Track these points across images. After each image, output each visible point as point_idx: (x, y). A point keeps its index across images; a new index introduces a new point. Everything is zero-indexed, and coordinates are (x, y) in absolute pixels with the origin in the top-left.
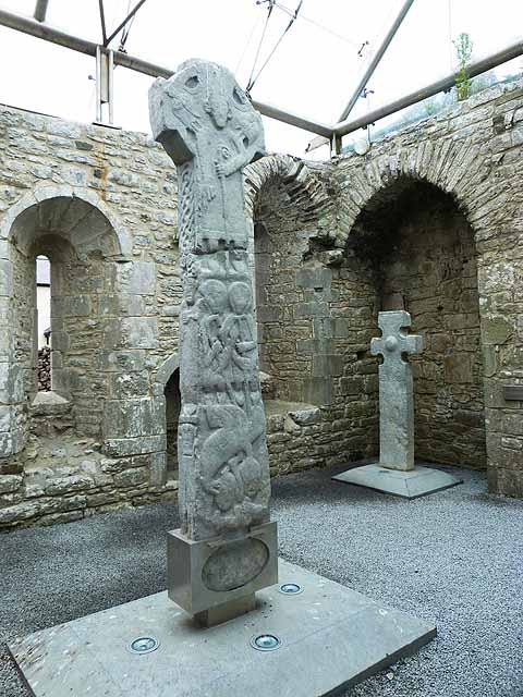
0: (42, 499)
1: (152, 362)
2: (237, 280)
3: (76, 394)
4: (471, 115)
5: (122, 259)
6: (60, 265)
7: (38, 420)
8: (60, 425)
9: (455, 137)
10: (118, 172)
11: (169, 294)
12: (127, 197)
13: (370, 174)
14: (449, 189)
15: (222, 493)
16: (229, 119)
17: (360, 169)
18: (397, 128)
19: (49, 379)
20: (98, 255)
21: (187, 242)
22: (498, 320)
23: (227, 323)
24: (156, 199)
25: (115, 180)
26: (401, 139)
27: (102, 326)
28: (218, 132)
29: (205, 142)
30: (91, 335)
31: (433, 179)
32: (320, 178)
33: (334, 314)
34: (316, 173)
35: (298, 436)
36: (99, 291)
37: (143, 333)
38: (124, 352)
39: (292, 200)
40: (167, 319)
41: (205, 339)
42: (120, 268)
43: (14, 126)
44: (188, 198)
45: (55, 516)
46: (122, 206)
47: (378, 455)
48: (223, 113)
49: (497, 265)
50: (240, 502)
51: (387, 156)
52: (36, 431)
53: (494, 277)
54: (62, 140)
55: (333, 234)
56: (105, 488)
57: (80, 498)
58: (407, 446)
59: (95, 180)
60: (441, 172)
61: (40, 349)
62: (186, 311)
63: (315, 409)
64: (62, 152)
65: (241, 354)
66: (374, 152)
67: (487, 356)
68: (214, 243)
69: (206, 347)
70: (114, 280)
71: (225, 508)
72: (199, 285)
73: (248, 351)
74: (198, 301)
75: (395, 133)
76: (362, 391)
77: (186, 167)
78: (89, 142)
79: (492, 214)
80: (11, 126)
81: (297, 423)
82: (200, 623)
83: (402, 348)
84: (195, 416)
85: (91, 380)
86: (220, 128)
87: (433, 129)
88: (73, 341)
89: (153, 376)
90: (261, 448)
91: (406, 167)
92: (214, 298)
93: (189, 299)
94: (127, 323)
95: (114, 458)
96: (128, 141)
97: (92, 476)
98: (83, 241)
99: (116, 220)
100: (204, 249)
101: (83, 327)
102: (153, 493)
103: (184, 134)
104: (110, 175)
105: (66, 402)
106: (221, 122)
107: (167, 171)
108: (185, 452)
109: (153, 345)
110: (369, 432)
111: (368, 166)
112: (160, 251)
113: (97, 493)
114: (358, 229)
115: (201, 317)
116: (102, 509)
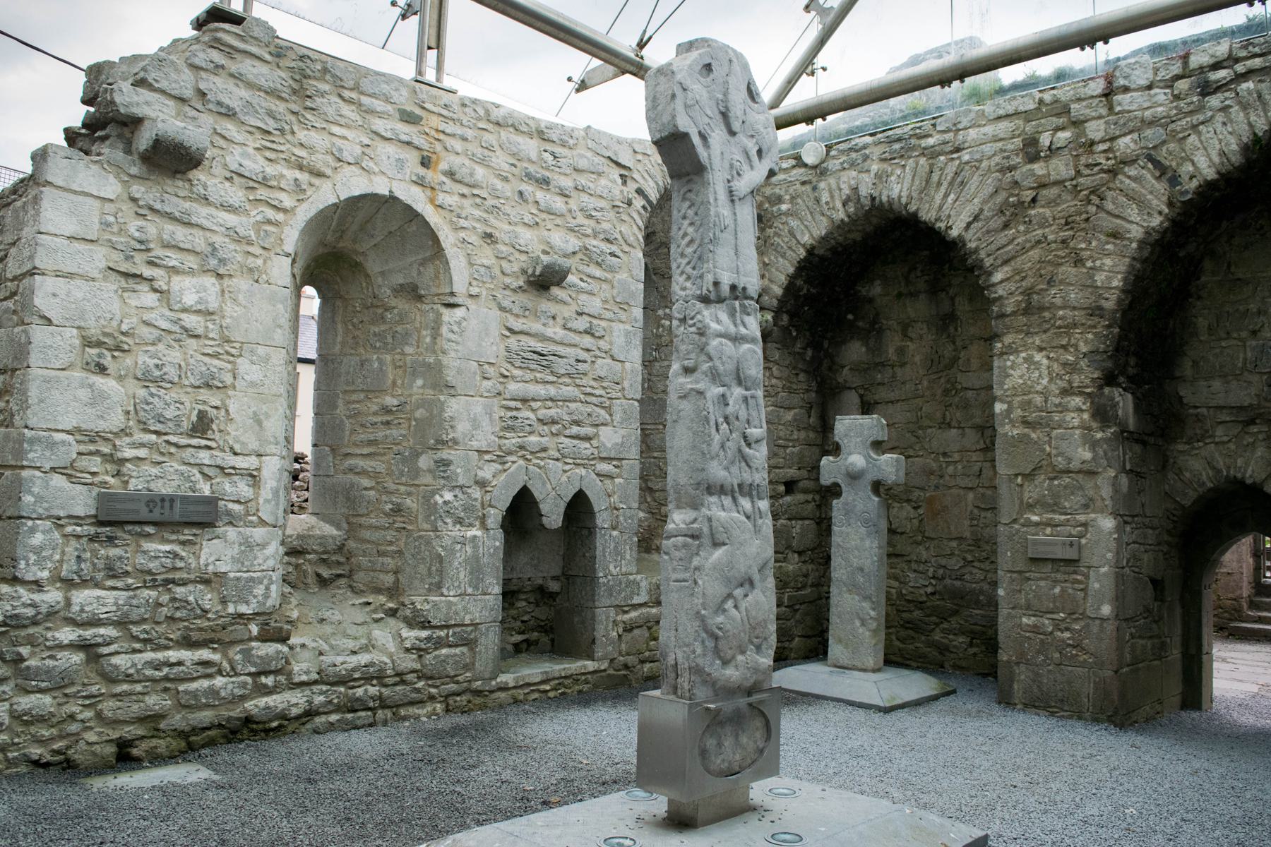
0: (316, 688)
1: (487, 472)
2: (748, 342)
4: (989, 130)
5: (452, 300)
6: (339, 303)
7: (293, 560)
9: (966, 158)
13: (825, 197)
14: (954, 233)
15: (726, 638)
17: (808, 188)
20: (413, 292)
22: (1023, 439)
24: (507, 209)
25: (451, 174)
30: (388, 423)
31: (927, 215)
36: (409, 350)
37: (476, 425)
38: (445, 454)
40: (513, 404)
42: (447, 315)
43: (315, 78)
45: (334, 718)
49: (1023, 355)
50: (743, 652)
51: (854, 173)
53: (1018, 372)
56: (410, 677)
57: (373, 690)
58: (874, 631)
59: (422, 171)
60: (940, 208)
64: (379, 125)
66: (833, 165)
67: (1003, 490)
70: (436, 334)
72: (707, 344)
73: (757, 441)
76: (789, 547)
77: (689, 181)
78: (418, 111)
79: (1017, 278)
80: (309, 77)
82: (679, 821)
83: (870, 477)
84: (695, 526)
85: (384, 498)
87: (931, 141)
88: (354, 431)
89: (488, 497)
91: (885, 193)
92: (723, 363)
94: (454, 406)
95: (424, 628)
96: (473, 114)
97: (391, 656)
99: (447, 238)
100: (713, 296)
101: (375, 408)
102: (478, 693)
103: (696, 140)
104: (443, 166)
105: (335, 532)
107: (525, 165)
108: (675, 576)
109: (489, 445)
110: (798, 616)
111: (822, 185)
112: (507, 292)
113: (395, 684)
114: (799, 282)
116: (402, 712)
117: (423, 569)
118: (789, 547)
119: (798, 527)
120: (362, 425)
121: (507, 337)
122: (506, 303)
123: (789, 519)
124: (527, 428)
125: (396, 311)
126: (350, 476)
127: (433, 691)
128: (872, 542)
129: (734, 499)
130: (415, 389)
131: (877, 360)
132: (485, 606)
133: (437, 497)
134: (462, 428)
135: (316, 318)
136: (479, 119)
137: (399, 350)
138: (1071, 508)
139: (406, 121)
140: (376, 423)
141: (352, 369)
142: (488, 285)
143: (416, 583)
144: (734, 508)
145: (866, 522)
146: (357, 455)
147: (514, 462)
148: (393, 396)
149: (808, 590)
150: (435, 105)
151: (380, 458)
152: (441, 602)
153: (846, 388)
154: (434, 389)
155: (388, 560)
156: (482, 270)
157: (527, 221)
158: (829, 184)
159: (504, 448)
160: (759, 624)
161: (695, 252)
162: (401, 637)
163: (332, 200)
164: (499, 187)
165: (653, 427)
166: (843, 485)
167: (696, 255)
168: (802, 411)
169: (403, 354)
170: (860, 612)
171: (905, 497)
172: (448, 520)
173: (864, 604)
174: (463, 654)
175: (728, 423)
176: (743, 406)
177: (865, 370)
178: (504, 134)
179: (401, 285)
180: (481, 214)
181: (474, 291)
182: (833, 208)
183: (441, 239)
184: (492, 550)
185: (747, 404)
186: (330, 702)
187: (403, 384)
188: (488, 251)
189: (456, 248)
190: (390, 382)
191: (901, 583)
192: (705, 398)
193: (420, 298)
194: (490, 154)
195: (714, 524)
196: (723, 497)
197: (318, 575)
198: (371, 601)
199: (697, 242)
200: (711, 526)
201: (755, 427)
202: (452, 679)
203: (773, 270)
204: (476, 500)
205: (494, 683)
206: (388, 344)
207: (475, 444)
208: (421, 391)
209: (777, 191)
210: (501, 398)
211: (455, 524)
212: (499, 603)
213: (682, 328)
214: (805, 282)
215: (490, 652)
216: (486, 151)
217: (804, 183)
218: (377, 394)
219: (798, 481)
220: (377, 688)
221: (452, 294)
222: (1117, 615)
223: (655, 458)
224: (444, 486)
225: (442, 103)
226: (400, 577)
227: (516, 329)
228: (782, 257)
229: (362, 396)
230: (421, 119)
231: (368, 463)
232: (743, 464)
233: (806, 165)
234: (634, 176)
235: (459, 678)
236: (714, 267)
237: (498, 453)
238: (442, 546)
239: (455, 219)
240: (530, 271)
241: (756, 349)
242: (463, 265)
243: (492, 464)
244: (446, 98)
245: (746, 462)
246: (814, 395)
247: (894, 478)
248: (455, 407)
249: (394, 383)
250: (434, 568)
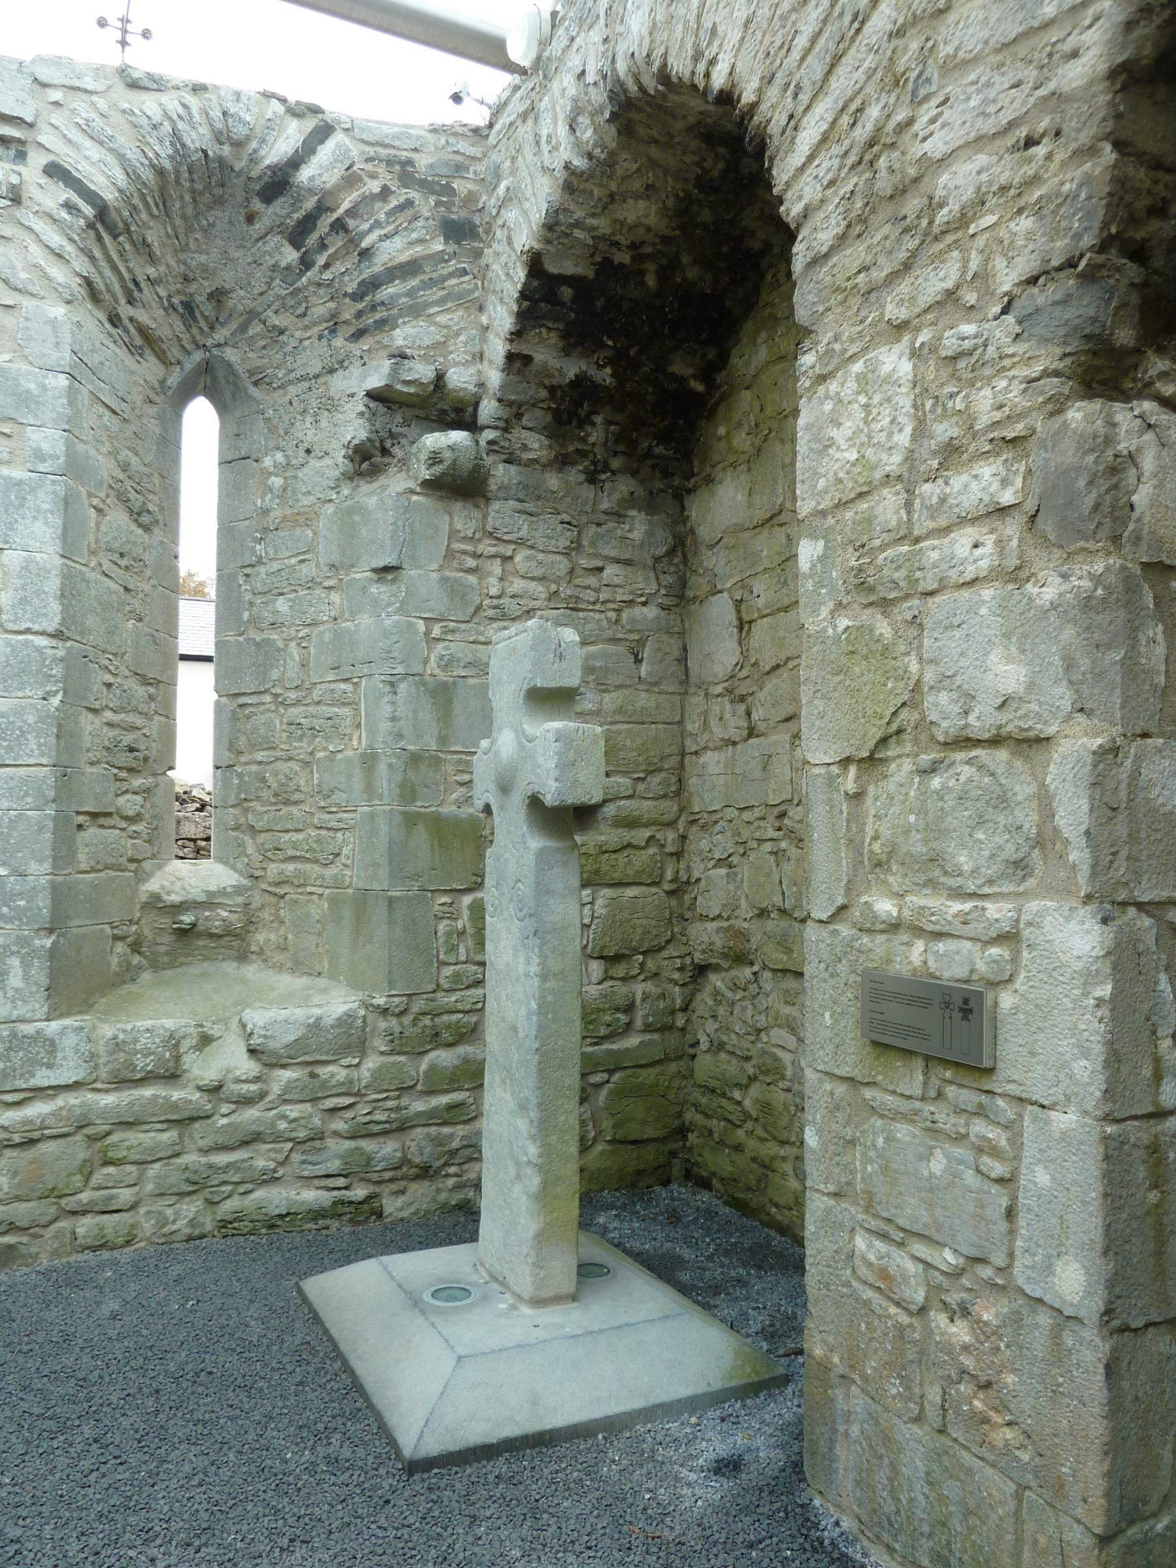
33: (447, 664)
34: (390, 162)
35: (247, 1101)
39: (306, 263)
119: (600, 902)
135: (212, 591)
138: (975, 872)
149: (632, 1041)
222: (1108, 1312)
223: (260, 763)
234: (42, 139)
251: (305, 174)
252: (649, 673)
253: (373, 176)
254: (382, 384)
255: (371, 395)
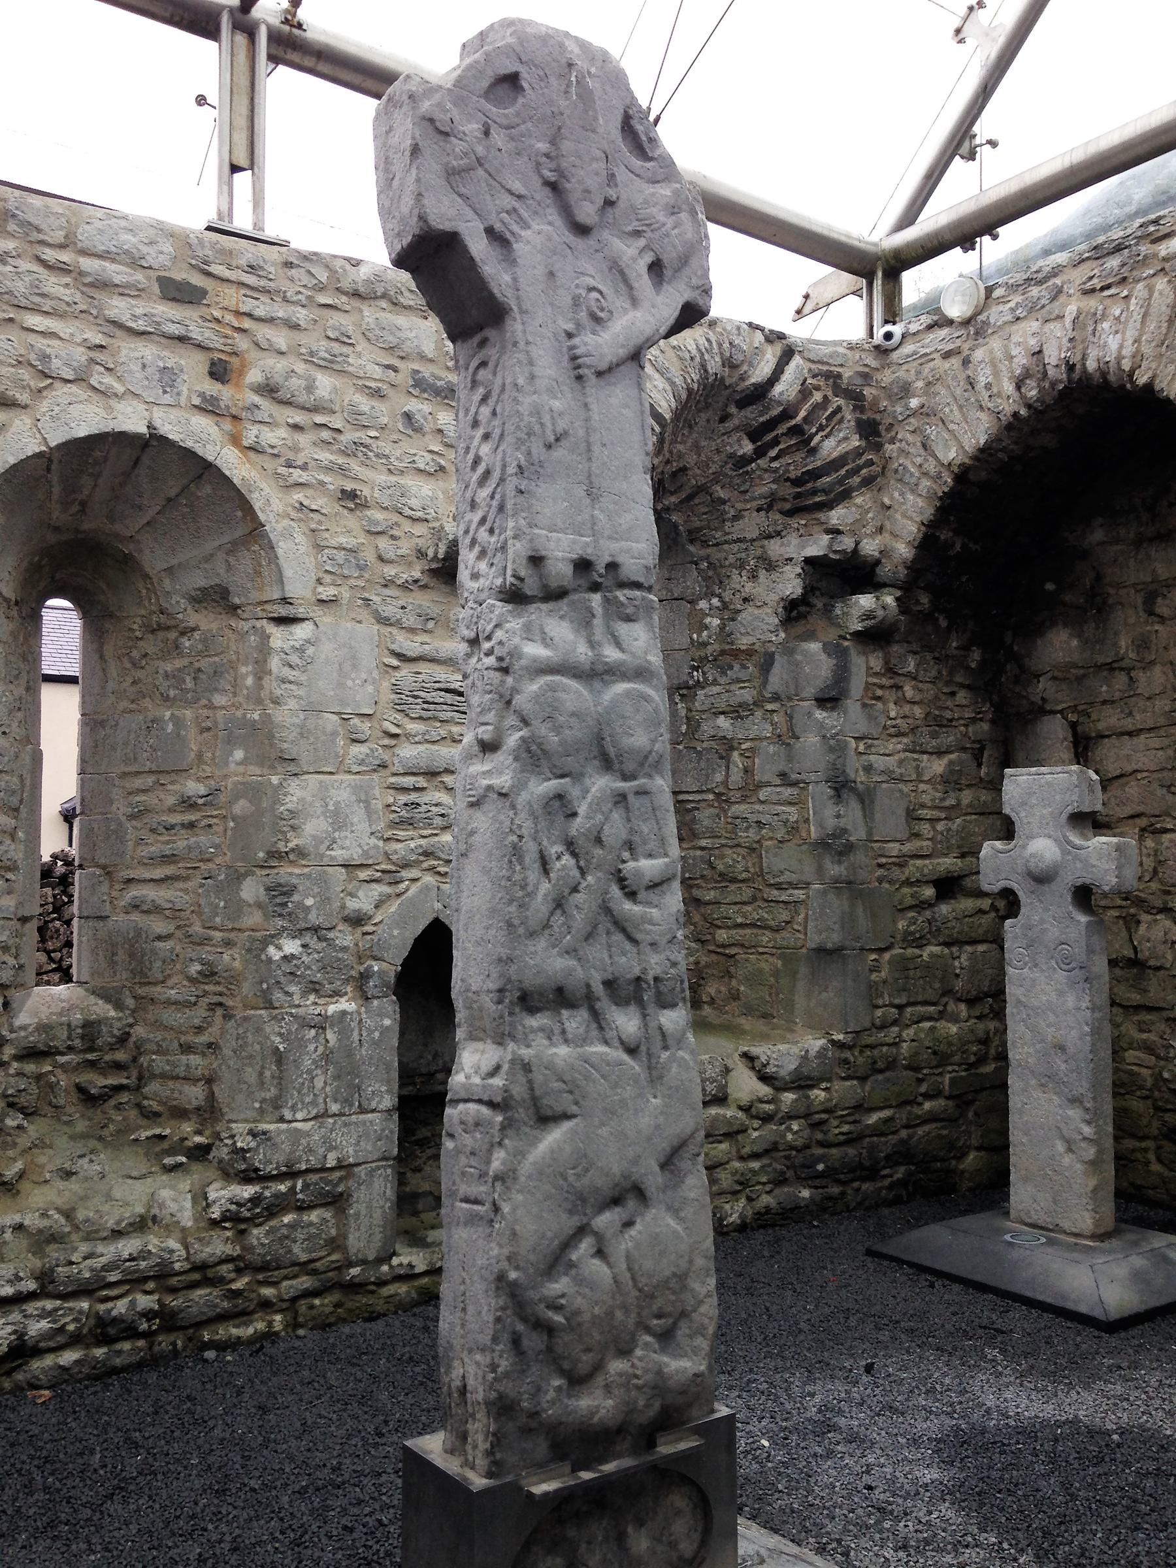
0: (32, 1307)
1: (363, 900)
3: (141, 991)
5: (283, 611)
7: (30, 1067)
8: (98, 1082)
10: (277, 366)
11: (417, 711)
12: (304, 439)
13: (983, 377)
16: (609, 203)
17: (955, 361)
18: (1063, 247)
19: (69, 944)
21: (483, 566)
23: (596, 807)
24: (385, 447)
25: (269, 390)
26: (1078, 276)
27: (223, 798)
28: (579, 243)
29: (540, 271)
30: (191, 826)
32: (838, 390)
34: (828, 375)
36: (220, 700)
37: (339, 820)
38: (287, 872)
39: (760, 453)
40: (409, 781)
41: (530, 848)
42: (278, 637)
44: (486, 437)
46: (289, 465)
47: (1006, 1183)
48: (592, 183)
50: (625, 1352)
51: (1035, 325)
52: (23, 1100)
54: (117, 272)
55: (870, 547)
57: (145, 1302)
59: (211, 387)
61: (46, 858)
62: (477, 768)
63: (815, 1044)
64: (118, 307)
65: (632, 895)
68: (560, 569)
69: (533, 874)
70: (262, 672)
71: (583, 1368)
72: (515, 690)
73: (654, 886)
74: (512, 740)
75: (1061, 258)
76: (948, 992)
77: (483, 343)
78: (197, 280)
81: (764, 1078)
83: (1071, 877)
84: (497, 1082)
86: (582, 230)
90: (691, 1181)
92: (557, 729)
93: (486, 733)
94: (297, 793)
96: (306, 280)
98: (174, 562)
100: (531, 587)
101: (171, 800)
102: (354, 1287)
103: (478, 246)
104: (254, 376)
106: (587, 212)
109: (366, 854)
114: (944, 535)
115: (520, 786)
117: (250, 1075)
118: (948, 992)
119: (964, 957)
120: (153, 831)
121: (395, 668)
122: (389, 611)
123: (946, 944)
124: (438, 821)
125: (197, 635)
126: (135, 917)
127: (268, 1292)
128: (1079, 999)
129: (596, 1016)
130: (232, 766)
131: (1101, 659)
132: (366, 1134)
133: (271, 950)
134: (313, 827)
136: (321, 288)
137: (204, 702)
139: (174, 300)
140: (172, 827)
141: (133, 736)
142: (353, 582)
143: (240, 1098)
144: (595, 1033)
145: (1066, 962)
146: (145, 881)
147: (414, 880)
148: (198, 780)
150: (230, 267)
151: (181, 885)
152: (279, 1132)
153: (1041, 710)
154: (262, 765)
155: (195, 1060)
156: (340, 556)
157: (422, 466)
158: (991, 352)
159: (394, 857)
160: (664, 1285)
161: (492, 497)
162: (206, 1199)
163: (33, 447)
164: (365, 408)
165: (698, 797)
166: (1020, 894)
167: (495, 503)
168: (964, 756)
169: (211, 707)
170: (1062, 1125)
171: (1158, 903)
172: (293, 989)
173: (1070, 1112)
174: (324, 1221)
175: (574, 855)
176: (616, 816)
177: (1080, 679)
178: (370, 314)
179: (203, 590)
180: (332, 458)
181: (326, 592)
182: (999, 395)
183: (257, 506)
184: (377, 1034)
185: (627, 809)
186: (62, 1330)
187: (213, 759)
188: (352, 521)
189: (286, 522)
190: (193, 755)
191: (1158, 1057)
192: (513, 807)
193: (234, 609)
194: (345, 349)
195: (538, 1076)
196: (565, 1013)
197: (80, 1089)
198: (167, 1132)
199: (496, 475)
200: (530, 1082)
201: (650, 856)
202: (305, 1267)
203: (898, 516)
204: (344, 949)
205: (385, 1268)
206: (187, 691)
207: (339, 854)
208: (241, 769)
209: (901, 373)
210: (387, 772)
211: (305, 994)
212: (394, 1125)
213: (474, 660)
214: (957, 533)
215: (377, 1214)
216: (336, 345)
217: (947, 355)
218: (174, 776)
219: (961, 877)
220: (156, 1297)
221: (285, 601)
223: (703, 849)
224: (284, 929)
225: (243, 262)
226: (216, 1089)
227: (409, 654)
228: (913, 491)
229: (150, 780)
230: (203, 293)
231: (162, 893)
232: (618, 937)
233: (950, 322)
235: (318, 1264)
236: (530, 526)
237: (384, 867)
238: (280, 1035)
239: (283, 470)
240: (431, 553)
241: (651, 692)
242: (303, 549)
243: (374, 886)
244: (249, 253)
245: (624, 931)
246: (986, 726)
247: (1114, 880)
248: (299, 793)
249: (200, 756)
250: (268, 1073)
251: (778, 389)
252: (987, 774)
253: (817, 388)
254: (821, 553)
255: (808, 561)
